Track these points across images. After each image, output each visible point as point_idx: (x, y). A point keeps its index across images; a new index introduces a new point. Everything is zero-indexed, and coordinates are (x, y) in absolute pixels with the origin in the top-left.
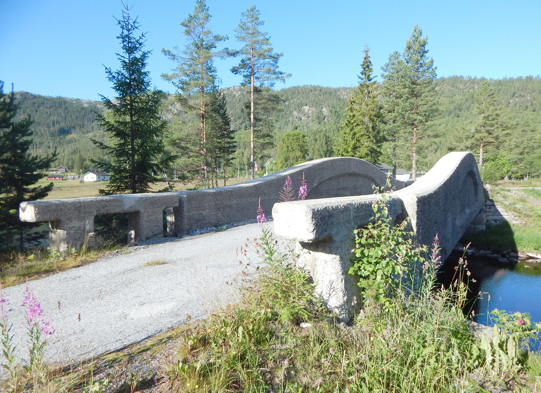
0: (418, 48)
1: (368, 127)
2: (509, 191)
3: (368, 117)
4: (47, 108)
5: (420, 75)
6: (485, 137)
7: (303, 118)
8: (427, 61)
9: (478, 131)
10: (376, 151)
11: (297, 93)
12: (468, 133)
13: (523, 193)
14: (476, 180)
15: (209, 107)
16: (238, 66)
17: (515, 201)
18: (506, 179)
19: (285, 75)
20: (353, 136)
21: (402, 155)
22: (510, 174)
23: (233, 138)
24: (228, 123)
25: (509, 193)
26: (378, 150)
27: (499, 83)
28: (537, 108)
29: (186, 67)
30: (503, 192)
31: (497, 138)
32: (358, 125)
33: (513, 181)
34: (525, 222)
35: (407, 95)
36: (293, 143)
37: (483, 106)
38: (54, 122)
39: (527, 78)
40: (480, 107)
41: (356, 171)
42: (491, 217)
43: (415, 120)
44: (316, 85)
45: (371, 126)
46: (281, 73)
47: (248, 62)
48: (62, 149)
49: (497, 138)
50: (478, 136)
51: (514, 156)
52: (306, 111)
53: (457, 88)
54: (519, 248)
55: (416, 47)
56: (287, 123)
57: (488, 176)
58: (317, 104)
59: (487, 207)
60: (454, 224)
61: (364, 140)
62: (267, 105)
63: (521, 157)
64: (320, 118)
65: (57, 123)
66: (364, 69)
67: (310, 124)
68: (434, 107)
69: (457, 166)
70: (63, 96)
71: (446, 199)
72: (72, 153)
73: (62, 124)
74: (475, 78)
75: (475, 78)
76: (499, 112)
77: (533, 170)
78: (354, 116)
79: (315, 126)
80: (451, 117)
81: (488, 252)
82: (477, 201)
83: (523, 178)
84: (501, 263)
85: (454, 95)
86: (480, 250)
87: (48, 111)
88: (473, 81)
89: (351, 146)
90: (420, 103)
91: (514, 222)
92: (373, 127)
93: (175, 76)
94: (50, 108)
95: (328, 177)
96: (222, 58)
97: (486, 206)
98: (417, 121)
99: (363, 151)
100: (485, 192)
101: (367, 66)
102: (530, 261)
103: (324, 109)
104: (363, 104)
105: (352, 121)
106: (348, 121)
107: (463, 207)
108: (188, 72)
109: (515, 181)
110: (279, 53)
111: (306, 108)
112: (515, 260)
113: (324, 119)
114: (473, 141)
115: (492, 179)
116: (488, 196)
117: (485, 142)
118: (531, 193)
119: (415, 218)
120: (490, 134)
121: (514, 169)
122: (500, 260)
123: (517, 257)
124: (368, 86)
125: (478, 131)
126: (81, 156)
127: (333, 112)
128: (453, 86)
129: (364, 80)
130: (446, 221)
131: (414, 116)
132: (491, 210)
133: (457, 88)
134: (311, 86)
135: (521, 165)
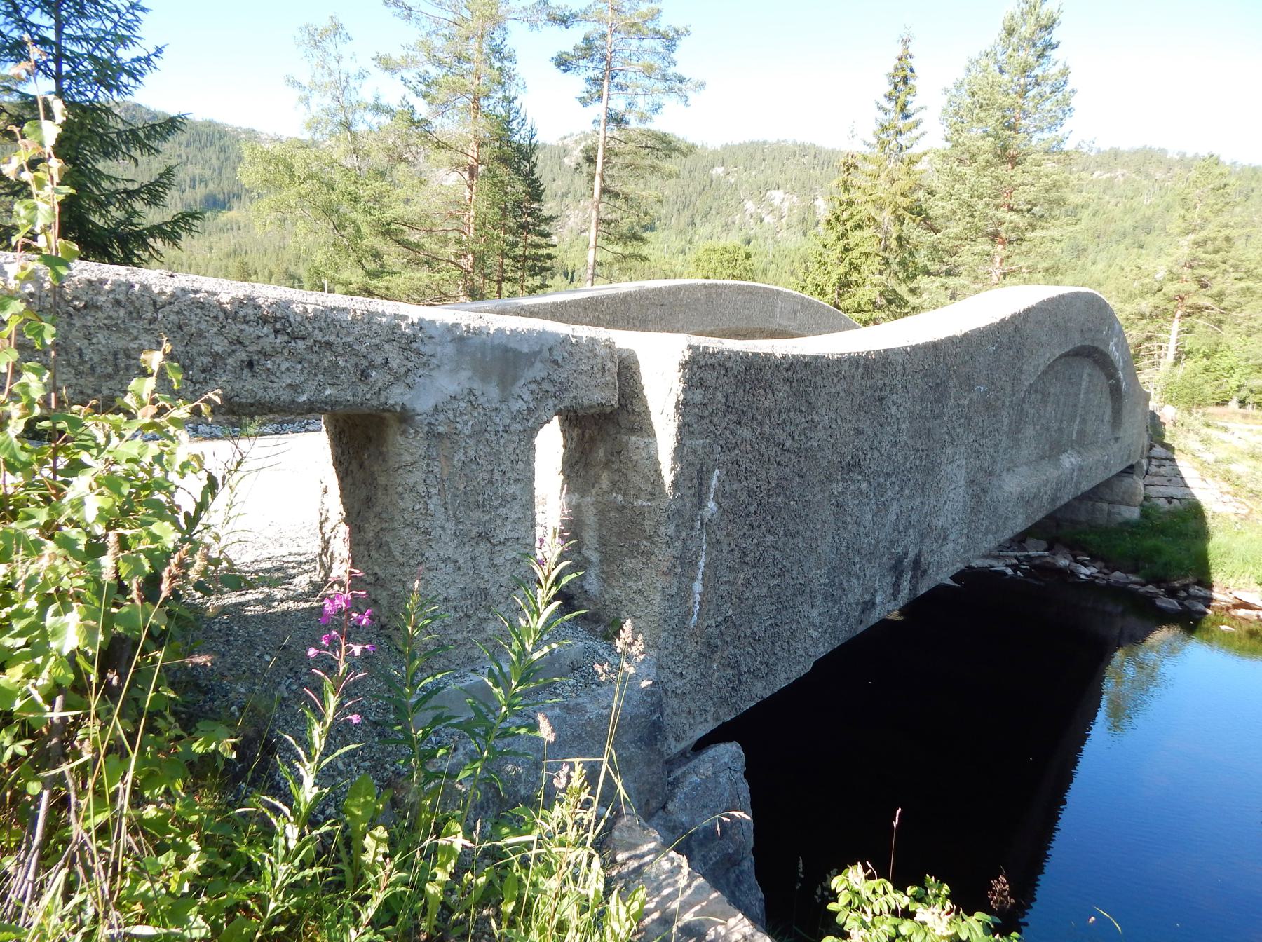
3: (890, 210)
4: (180, 144)
5: (1029, 106)
6: (1188, 293)
7: (768, 219)
8: (1054, 71)
10: (902, 299)
11: (758, 156)
12: (1147, 280)
14: (1118, 380)
15: (487, 150)
16: (570, 50)
17: (1235, 456)
18: (1234, 404)
19: (689, 84)
20: (842, 253)
22: (1244, 393)
23: (547, 235)
24: (540, 195)
29: (438, 42)
32: (858, 227)
34: (1247, 511)
35: (989, 156)
36: (720, 269)
38: (193, 180)
40: (1188, 216)
42: (1159, 490)
44: (808, 141)
45: (894, 236)
46: (681, 80)
47: (598, 43)
48: (207, 243)
49: (1219, 297)
50: (1171, 289)
52: (777, 202)
53: (1147, 176)
54: (1216, 577)
56: (727, 228)
58: (805, 188)
59: (1154, 462)
62: (636, 161)
65: (201, 181)
67: (783, 234)
68: (1054, 195)
70: (218, 120)
72: (229, 256)
73: (211, 186)
76: (1233, 233)
78: (850, 203)
80: (1122, 247)
81: (1133, 578)
82: (1117, 439)
84: (1161, 610)
85: (1137, 192)
87: (182, 150)
89: (834, 277)
90: (1019, 179)
92: (899, 238)
93: (407, 63)
94: (188, 145)
96: (533, 25)
98: (1004, 227)
102: (1242, 612)
104: (883, 176)
105: (845, 217)
108: (441, 55)
110: (680, 26)
111: (777, 195)
112: (1200, 607)
113: (817, 225)
114: (1158, 299)
115: (1190, 398)
116: (1162, 436)
120: (1204, 286)
122: (1158, 603)
123: (1208, 601)
125: (1174, 277)
126: (243, 263)
128: (1138, 171)
129: (892, 115)
131: (1003, 214)
132: (1163, 470)
133: (1147, 176)
134: (795, 143)
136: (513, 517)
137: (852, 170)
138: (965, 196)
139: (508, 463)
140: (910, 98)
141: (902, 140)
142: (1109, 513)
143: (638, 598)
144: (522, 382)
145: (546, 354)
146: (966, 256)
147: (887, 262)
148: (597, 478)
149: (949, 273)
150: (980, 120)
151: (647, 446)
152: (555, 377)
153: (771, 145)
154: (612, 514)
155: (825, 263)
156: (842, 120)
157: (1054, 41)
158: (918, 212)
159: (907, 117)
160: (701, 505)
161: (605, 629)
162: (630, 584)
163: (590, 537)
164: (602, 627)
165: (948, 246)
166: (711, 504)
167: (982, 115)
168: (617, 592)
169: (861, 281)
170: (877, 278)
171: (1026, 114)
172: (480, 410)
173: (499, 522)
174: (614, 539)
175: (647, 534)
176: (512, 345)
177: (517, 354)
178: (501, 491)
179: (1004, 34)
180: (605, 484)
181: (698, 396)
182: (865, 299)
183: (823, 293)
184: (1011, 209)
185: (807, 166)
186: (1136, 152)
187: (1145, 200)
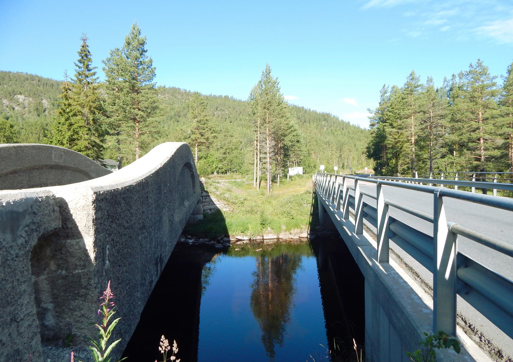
0: (137, 46)
1: (88, 120)
2: (218, 183)
3: (88, 108)
5: (140, 72)
7: (16, 108)
8: (147, 60)
9: (193, 133)
10: (98, 145)
12: (185, 134)
13: (228, 184)
14: (193, 172)
18: (215, 173)
20: (69, 126)
21: (125, 149)
22: (218, 169)
25: (219, 185)
26: (101, 144)
27: (207, 98)
28: (233, 121)
30: (214, 184)
31: (207, 139)
32: (75, 115)
33: (220, 175)
37: (196, 112)
39: (225, 96)
41: (61, 162)
43: (137, 115)
45: (91, 119)
49: (207, 139)
50: (193, 137)
51: (219, 155)
52: (21, 100)
54: (230, 233)
55: (135, 43)
57: (202, 172)
58: (35, 95)
59: (204, 198)
60: (171, 222)
61: (83, 133)
63: (224, 156)
64: (39, 111)
66: (82, 58)
67: (27, 115)
68: (154, 105)
69: (173, 153)
71: (160, 193)
74: (190, 91)
75: (190, 91)
76: (208, 118)
77: (233, 166)
78: (70, 105)
79: (32, 118)
81: (206, 240)
82: (195, 192)
83: (226, 172)
85: (174, 103)
86: (199, 239)
88: (188, 94)
89: (67, 137)
91: (225, 210)
92: (93, 120)
95: (10, 169)
97: (202, 197)
99: (82, 144)
100: (201, 184)
101: (85, 55)
102: (239, 243)
103: (44, 101)
104: (82, 94)
105: (68, 110)
106: (62, 109)
107: (183, 200)
109: (222, 175)
112: (228, 244)
113: (44, 111)
115: (206, 174)
116: (204, 188)
117: (199, 143)
118: (234, 184)
119: (92, 232)
120: (202, 136)
121: (220, 165)
124: (87, 76)
125: (193, 133)
127: (56, 105)
130: (160, 221)
131: (136, 111)
133: (176, 97)
134: (27, 74)
135: (225, 162)
136: (25, 302)
137: (68, 91)
138: (121, 104)
139: (19, 274)
140: (90, 63)
141: (89, 80)
142: (194, 218)
143: (82, 319)
144: (21, 227)
145: (30, 210)
146: (124, 126)
147: (89, 130)
148: (47, 265)
149: (118, 134)
150: (122, 75)
151: (78, 243)
152: (35, 220)
153: (14, 74)
154: (59, 281)
155: (61, 131)
156: (61, 69)
157: (145, 49)
158: (100, 109)
159: (89, 70)
160: (104, 264)
161: (63, 342)
162: (76, 313)
163: (46, 296)
164: (61, 341)
165: (116, 124)
166: (107, 262)
167: (123, 74)
168: (68, 320)
169: (79, 138)
170: (86, 137)
171: (139, 75)
172: (4, 249)
173: (19, 308)
174: (62, 294)
175: (83, 286)
176: (15, 209)
177: (18, 213)
178: (18, 290)
179: (126, 44)
180: (53, 266)
181: (100, 215)
182: (83, 146)
183: (62, 144)
184: (139, 110)
185: (35, 85)
186: (171, 89)
187: (176, 106)
